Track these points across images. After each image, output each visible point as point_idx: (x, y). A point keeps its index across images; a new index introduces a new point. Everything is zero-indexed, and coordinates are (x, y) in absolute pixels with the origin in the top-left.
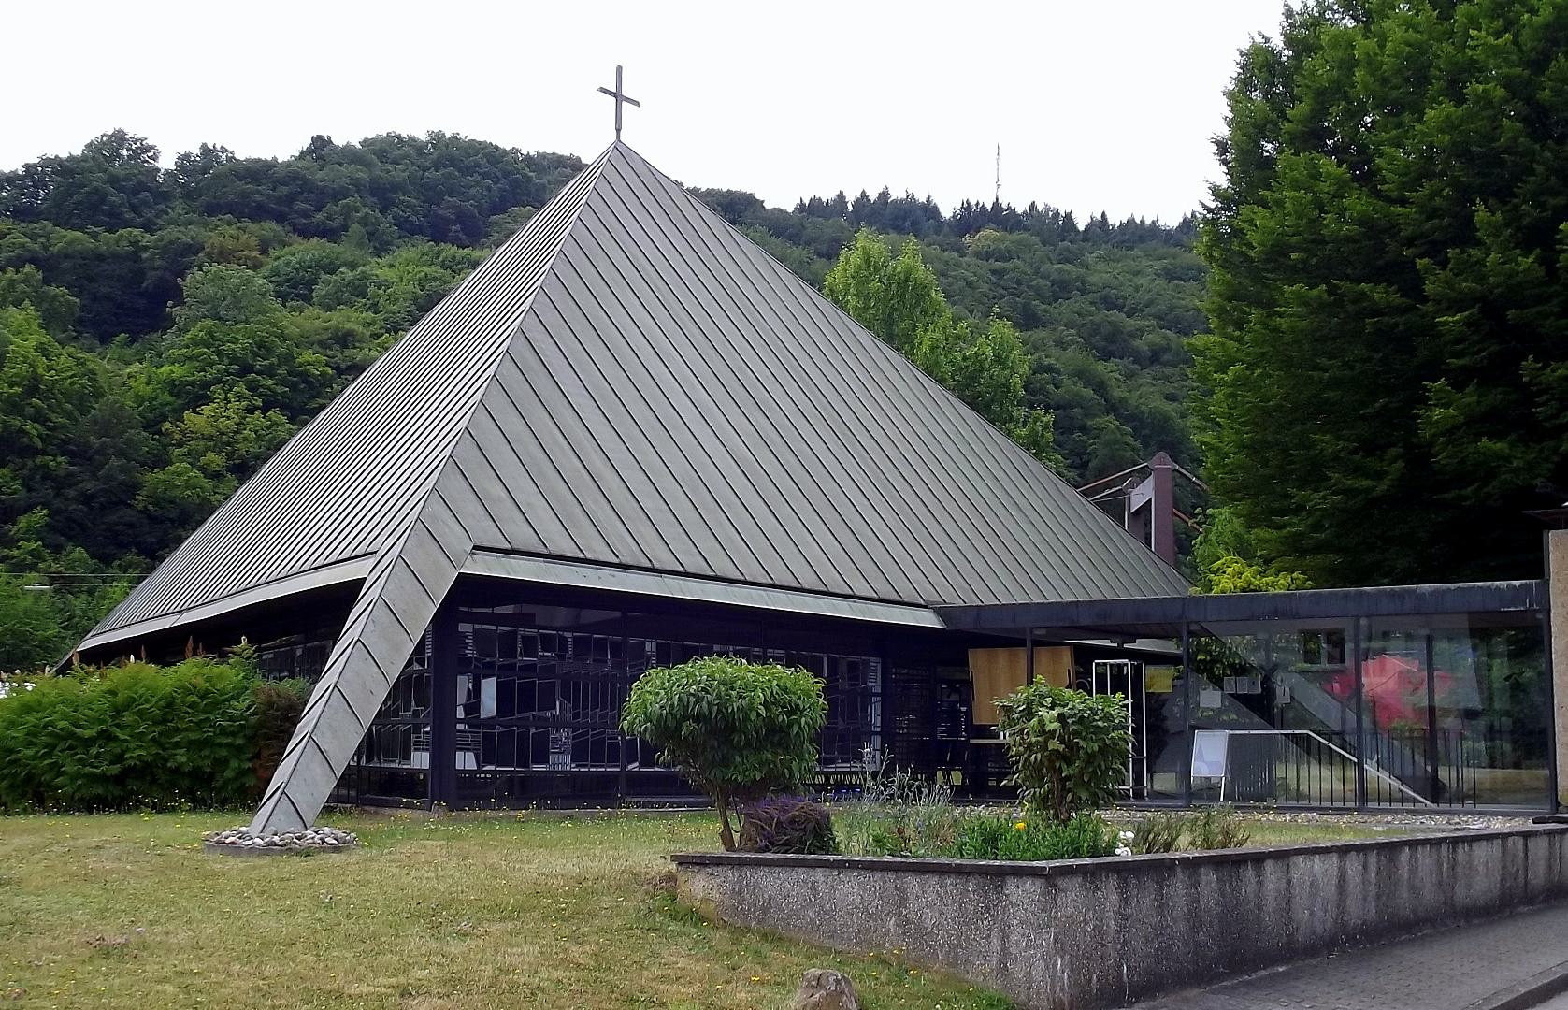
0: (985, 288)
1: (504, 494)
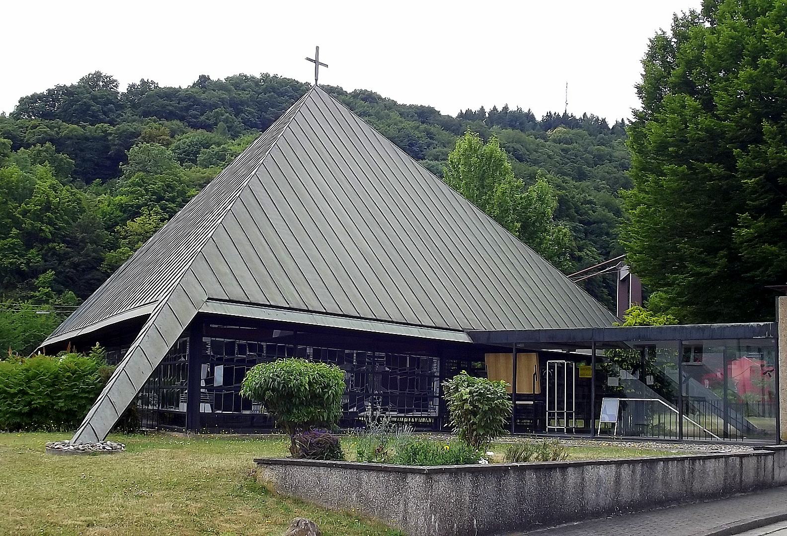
0: (558, 158)
1: (228, 271)
